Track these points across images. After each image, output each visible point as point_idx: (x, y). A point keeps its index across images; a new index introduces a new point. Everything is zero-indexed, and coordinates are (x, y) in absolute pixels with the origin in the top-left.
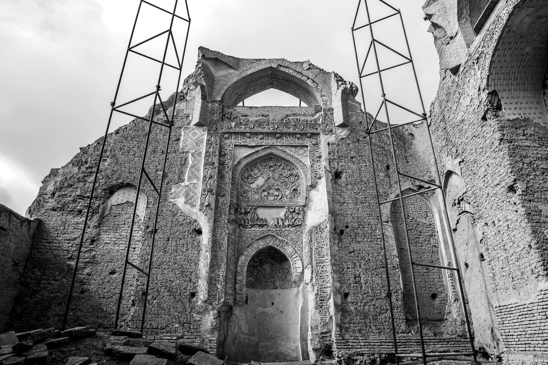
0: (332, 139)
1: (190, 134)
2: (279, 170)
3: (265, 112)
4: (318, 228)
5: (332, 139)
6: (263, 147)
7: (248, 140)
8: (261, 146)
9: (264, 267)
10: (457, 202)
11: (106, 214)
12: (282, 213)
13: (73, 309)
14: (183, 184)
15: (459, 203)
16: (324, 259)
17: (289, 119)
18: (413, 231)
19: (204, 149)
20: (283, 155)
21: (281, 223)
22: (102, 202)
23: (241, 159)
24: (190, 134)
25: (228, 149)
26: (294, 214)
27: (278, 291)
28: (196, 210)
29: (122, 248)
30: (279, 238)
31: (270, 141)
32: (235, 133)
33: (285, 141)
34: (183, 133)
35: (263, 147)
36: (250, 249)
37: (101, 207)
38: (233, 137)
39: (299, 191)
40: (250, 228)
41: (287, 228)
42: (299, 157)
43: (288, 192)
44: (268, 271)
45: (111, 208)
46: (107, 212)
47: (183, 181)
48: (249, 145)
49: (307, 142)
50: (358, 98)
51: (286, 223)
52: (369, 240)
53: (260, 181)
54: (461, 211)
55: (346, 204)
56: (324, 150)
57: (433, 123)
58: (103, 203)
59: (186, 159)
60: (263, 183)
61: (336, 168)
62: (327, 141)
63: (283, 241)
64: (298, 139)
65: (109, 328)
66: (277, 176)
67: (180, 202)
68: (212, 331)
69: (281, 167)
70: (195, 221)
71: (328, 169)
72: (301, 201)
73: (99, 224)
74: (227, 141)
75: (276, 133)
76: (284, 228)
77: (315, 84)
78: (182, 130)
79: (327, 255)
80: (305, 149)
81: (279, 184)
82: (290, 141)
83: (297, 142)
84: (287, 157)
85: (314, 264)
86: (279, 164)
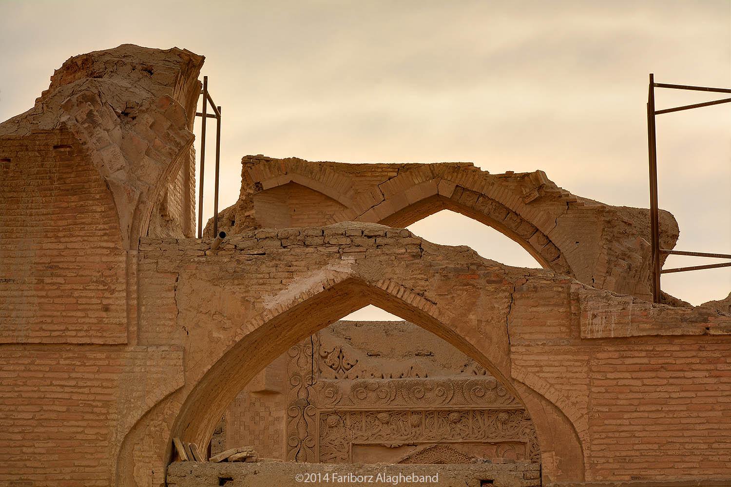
7: (386, 430)
32: (353, 413)
38: (348, 422)
48: (387, 443)
75: (450, 412)
77: (553, 250)
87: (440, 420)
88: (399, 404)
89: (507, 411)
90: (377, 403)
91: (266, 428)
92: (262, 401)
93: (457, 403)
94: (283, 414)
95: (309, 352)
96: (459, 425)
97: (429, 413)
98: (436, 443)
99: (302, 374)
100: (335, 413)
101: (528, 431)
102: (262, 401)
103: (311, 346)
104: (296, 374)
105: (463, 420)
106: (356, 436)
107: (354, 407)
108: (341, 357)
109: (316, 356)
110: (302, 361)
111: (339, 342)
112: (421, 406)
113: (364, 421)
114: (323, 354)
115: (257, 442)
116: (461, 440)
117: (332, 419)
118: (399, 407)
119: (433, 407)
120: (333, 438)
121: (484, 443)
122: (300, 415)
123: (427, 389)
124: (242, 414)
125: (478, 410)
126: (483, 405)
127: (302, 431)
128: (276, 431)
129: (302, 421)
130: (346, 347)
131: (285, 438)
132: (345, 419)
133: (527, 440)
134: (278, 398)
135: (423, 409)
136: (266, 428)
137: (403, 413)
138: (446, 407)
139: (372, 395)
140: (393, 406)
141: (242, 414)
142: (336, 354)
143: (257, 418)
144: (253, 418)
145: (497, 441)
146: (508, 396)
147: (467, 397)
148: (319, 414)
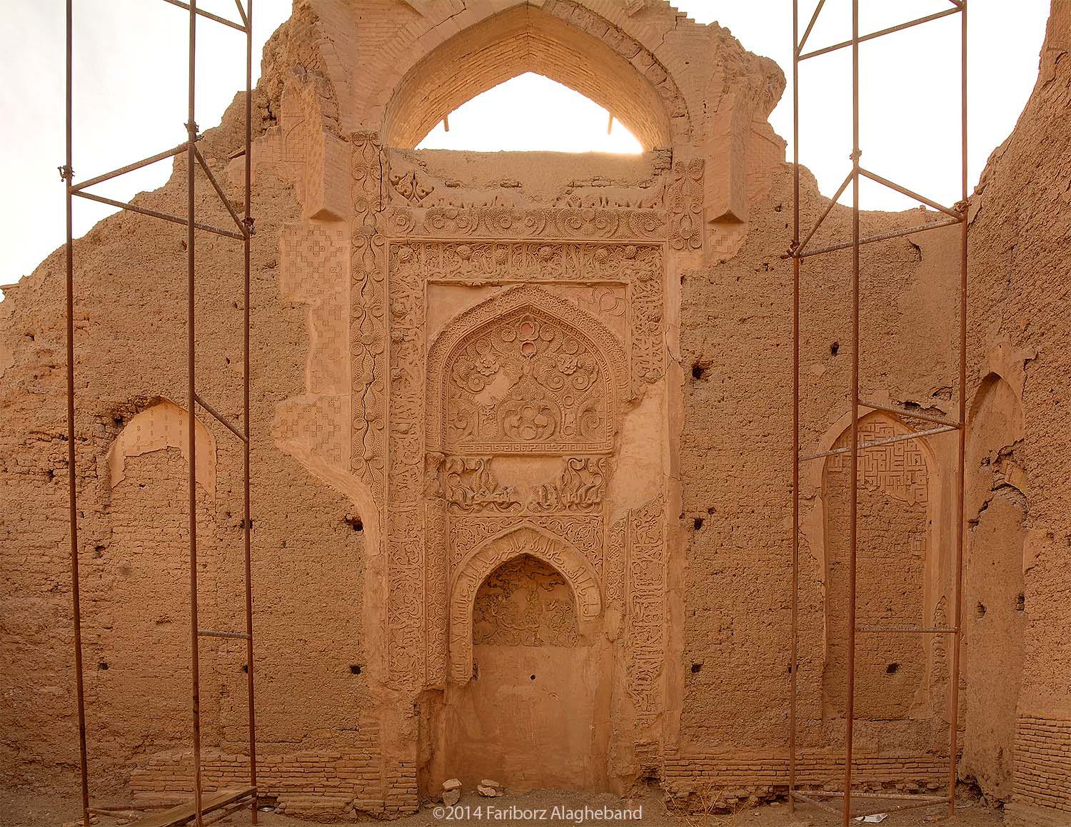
0: (690, 262)
1: (304, 249)
2: (549, 353)
3: (510, 170)
4: (643, 516)
5: (690, 262)
6: (506, 288)
7: (466, 266)
8: (498, 284)
9: (512, 597)
10: (995, 456)
11: (115, 482)
12: (555, 469)
13: (92, 703)
14: (301, 400)
15: (998, 461)
16: (651, 587)
17: (576, 199)
18: (870, 519)
19: (347, 294)
20: (559, 312)
21: (552, 498)
22: (99, 449)
23: (448, 326)
24: (304, 249)
25: (413, 294)
26: (584, 474)
27: (544, 650)
28: (341, 470)
29: (175, 565)
30: (548, 534)
31: (526, 268)
32: (430, 245)
33: (567, 266)
34: (282, 247)
35: (506, 288)
36: (479, 563)
37: (101, 461)
38: (423, 257)
39: (598, 415)
40: (479, 511)
41: (567, 512)
42: (601, 319)
43: (570, 418)
44: (523, 605)
45: (126, 465)
46: (118, 476)
47: (302, 390)
48: (469, 282)
49: (626, 271)
50: (779, 119)
51: (567, 499)
52: (762, 544)
53: (500, 386)
54: (1001, 482)
55: (714, 453)
56: (673, 295)
57: (981, 223)
58: (104, 453)
59: (302, 327)
60: (506, 392)
61: (697, 354)
62: (680, 271)
63: (558, 542)
64: (602, 262)
65: (180, 739)
66: (542, 371)
67: (299, 446)
68: (403, 742)
69: (554, 345)
70: (344, 498)
71: (678, 356)
72: (601, 442)
73: (106, 507)
74: (407, 270)
75: (541, 245)
76: (560, 510)
77: (659, 71)
78: (279, 232)
79: (660, 579)
80: (620, 292)
81: (549, 394)
82: (582, 267)
83: (599, 273)
84: (568, 318)
85: (629, 599)
86: (548, 337)
87: (529, 258)
88: (482, 234)
89: (606, 247)
90: (457, 234)
91: (327, 259)
92: (322, 229)
93: (550, 234)
94: (347, 244)
95: (377, 174)
96: (550, 264)
97: (518, 247)
98: (523, 282)
99: (369, 198)
100: (407, 244)
101: (629, 272)
102: (322, 229)
103: (379, 167)
104: (361, 200)
105: (556, 257)
106: (431, 272)
107: (430, 237)
108: (414, 184)
109: (385, 179)
110: (369, 184)
111: (410, 167)
112: (507, 237)
113: (441, 257)
114: (394, 179)
115: (316, 275)
116: (553, 280)
117: (404, 252)
118: (482, 237)
119: (520, 239)
120: (406, 274)
121: (580, 284)
122: (366, 245)
123: (514, 218)
124: (331, 122)
125: (574, 245)
126: (578, 237)
127: (368, 262)
128: (339, 263)
129: (369, 251)
130: (421, 175)
131: (348, 271)
132: (420, 254)
133: (629, 281)
134: (340, 226)
135: (508, 240)
136: (327, 259)
137: (486, 246)
138: (536, 238)
139: (452, 224)
140: (474, 237)
141: (331, 122)
142: (409, 179)
143: (316, 249)
144: (311, 249)
145: (596, 281)
146: (607, 229)
147: (561, 229)
148: (388, 244)
